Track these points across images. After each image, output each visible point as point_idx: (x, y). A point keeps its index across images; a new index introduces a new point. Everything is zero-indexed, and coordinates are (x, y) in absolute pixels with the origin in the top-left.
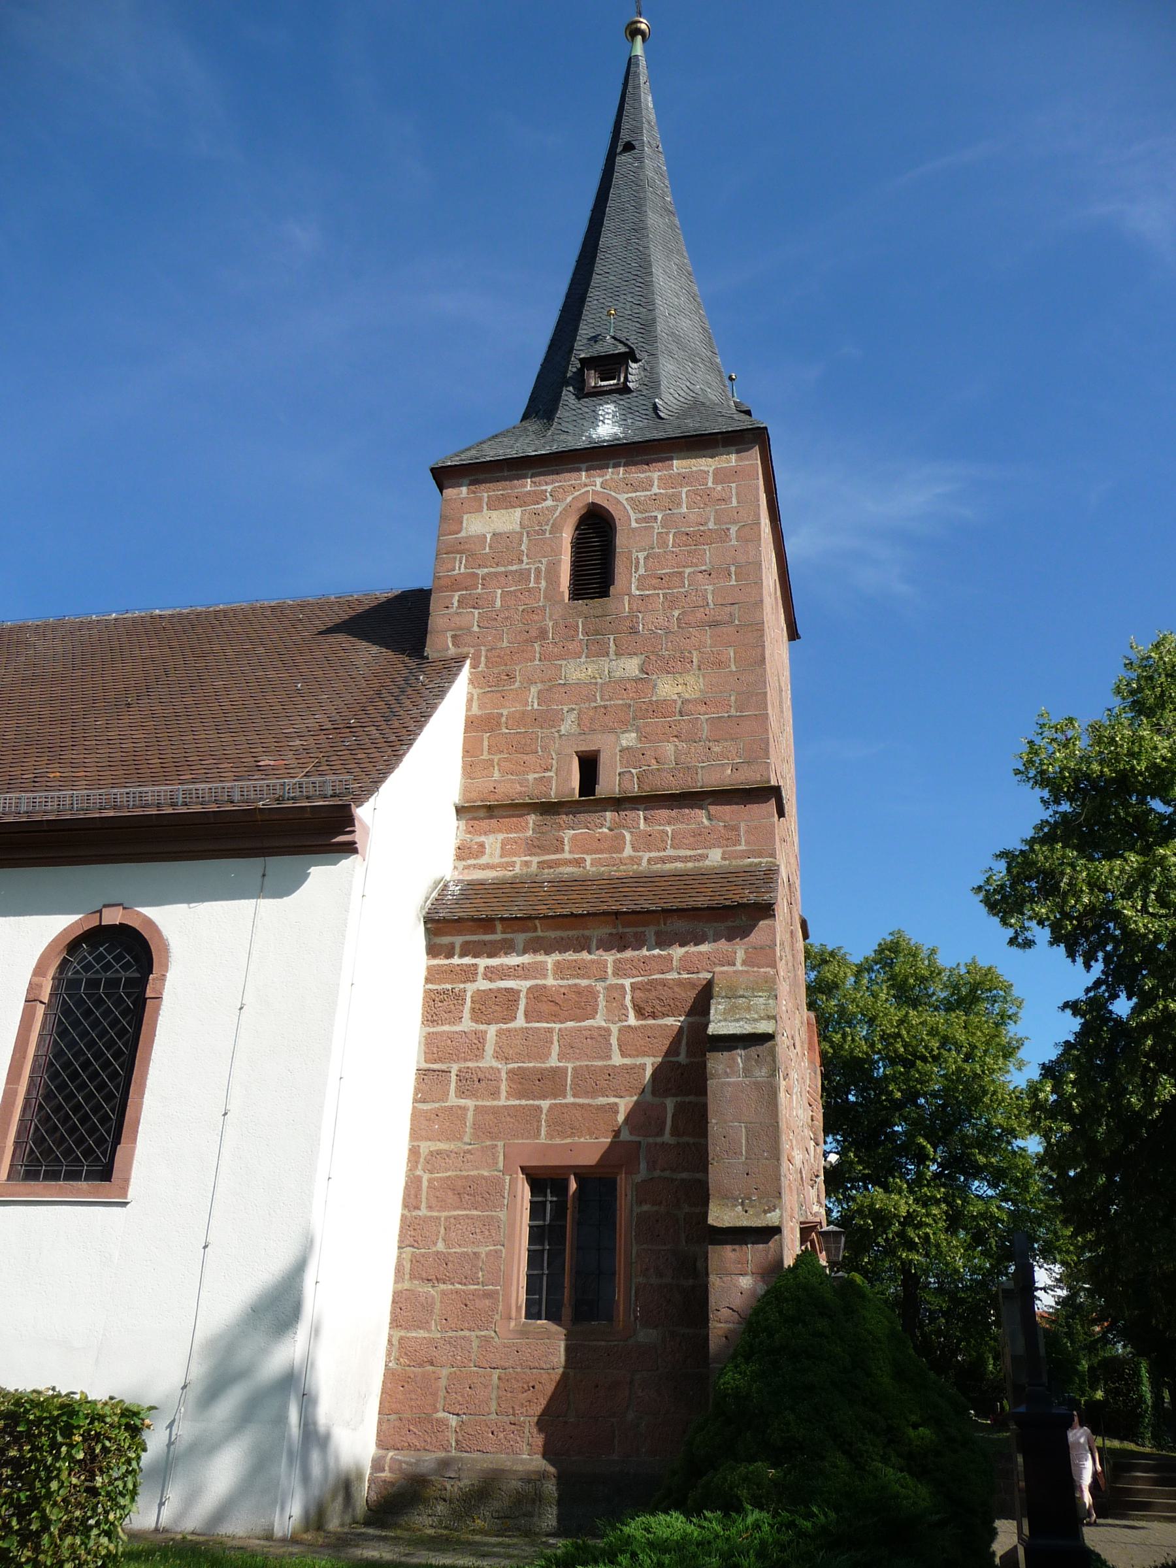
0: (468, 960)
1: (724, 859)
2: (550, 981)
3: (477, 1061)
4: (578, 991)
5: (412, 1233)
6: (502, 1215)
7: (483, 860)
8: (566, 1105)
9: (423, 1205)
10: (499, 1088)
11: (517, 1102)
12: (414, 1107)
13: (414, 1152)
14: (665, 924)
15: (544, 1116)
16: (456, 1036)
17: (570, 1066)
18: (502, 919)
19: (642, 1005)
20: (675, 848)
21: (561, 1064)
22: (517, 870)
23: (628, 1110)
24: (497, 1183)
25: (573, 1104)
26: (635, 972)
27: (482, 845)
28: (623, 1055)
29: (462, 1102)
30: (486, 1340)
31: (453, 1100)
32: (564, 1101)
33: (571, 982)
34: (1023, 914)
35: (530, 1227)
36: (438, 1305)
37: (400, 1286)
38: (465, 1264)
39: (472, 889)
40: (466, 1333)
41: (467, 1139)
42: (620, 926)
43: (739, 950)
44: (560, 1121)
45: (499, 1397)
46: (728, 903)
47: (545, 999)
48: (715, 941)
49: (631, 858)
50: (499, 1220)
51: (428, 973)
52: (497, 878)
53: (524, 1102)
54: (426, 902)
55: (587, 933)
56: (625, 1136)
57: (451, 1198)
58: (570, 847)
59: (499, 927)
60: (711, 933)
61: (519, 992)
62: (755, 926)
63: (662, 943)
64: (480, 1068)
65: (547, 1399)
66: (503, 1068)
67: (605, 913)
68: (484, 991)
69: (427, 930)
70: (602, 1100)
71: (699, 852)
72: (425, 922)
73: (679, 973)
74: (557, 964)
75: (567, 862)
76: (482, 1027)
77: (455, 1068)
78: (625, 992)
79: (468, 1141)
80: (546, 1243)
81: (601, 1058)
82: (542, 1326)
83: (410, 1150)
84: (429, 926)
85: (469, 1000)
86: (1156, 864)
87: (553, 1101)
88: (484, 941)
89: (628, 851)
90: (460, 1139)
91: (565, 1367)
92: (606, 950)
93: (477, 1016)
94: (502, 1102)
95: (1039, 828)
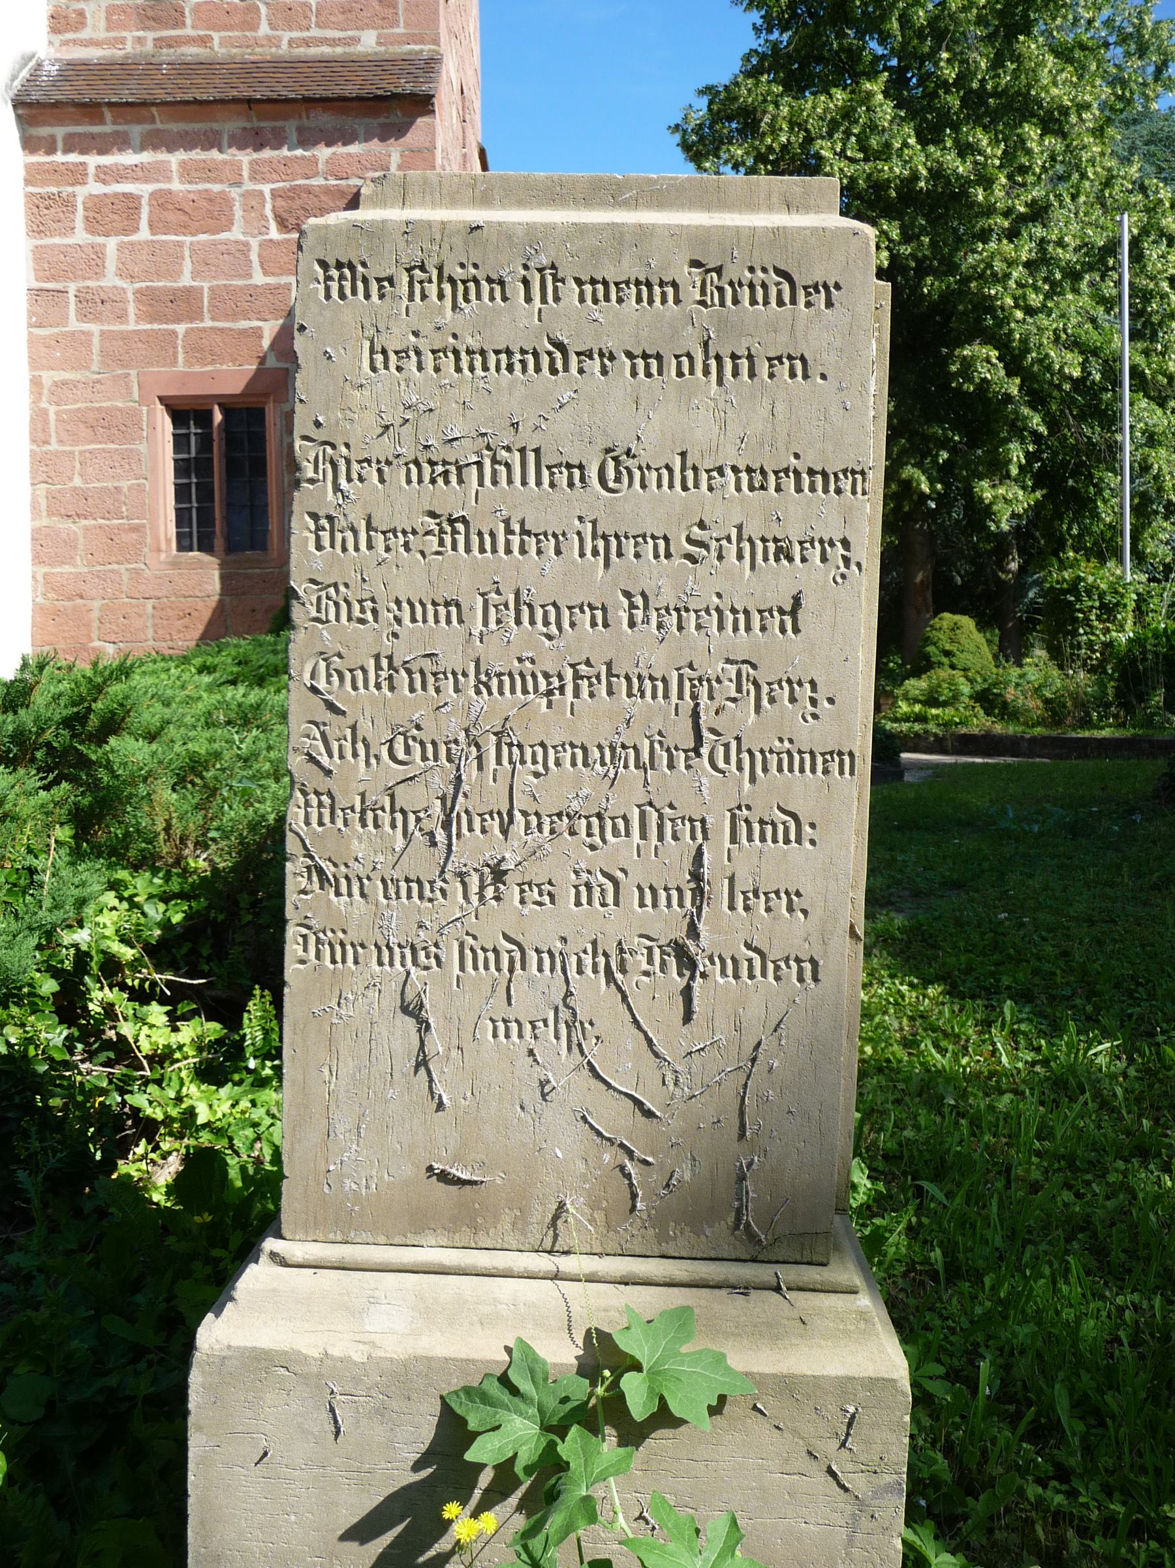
0: (74, 158)
1: (379, 43)
2: (176, 186)
3: (97, 280)
4: (210, 198)
5: (44, 469)
6: (142, 448)
7: (85, 34)
8: (204, 330)
9: (53, 440)
10: (126, 310)
11: (149, 327)
12: (30, 333)
13: (36, 382)
14: (308, 118)
15: (180, 342)
16: (69, 249)
17: (206, 285)
18: (110, 105)
19: (285, 215)
20: (320, 27)
21: (195, 284)
22: (129, 48)
23: (273, 335)
24: (134, 415)
25: (211, 328)
26: (274, 176)
27: (81, 14)
28: (266, 273)
29: (85, 327)
30: (137, 572)
31: (74, 324)
32: (201, 325)
33: (202, 186)
34: (719, 158)
35: (176, 461)
36: (81, 541)
37: (37, 524)
38: (106, 498)
39: (72, 70)
40: (115, 567)
41: (95, 368)
42: (254, 119)
43: (393, 153)
44: (198, 348)
45: (155, 625)
46: (380, 92)
47: (171, 207)
48: (366, 141)
49: (268, 38)
50: (139, 453)
51: (27, 172)
52: (103, 58)
53: (156, 326)
54: (13, 80)
55: (216, 126)
56: (272, 362)
57: (84, 432)
58: (193, 21)
59: (108, 116)
60: (361, 131)
61: (139, 197)
62: (412, 123)
63: (306, 141)
64: (101, 287)
65: (204, 624)
66: (130, 288)
67: (235, 101)
68: (97, 196)
69: (19, 117)
70: (244, 324)
71: (350, 33)
72: (14, 106)
73: (326, 179)
74: (183, 164)
75: (190, 40)
76: (101, 240)
77: (72, 288)
78: (264, 200)
79: (97, 370)
80: (193, 476)
81: (241, 277)
82: (194, 557)
83: (31, 380)
84: (20, 112)
85: (80, 207)
86: (862, 103)
87: (190, 325)
88: (91, 134)
89: (264, 29)
90: (87, 368)
91: (221, 595)
92: (240, 148)
93: (93, 225)
94: (132, 326)
95: (747, 58)
